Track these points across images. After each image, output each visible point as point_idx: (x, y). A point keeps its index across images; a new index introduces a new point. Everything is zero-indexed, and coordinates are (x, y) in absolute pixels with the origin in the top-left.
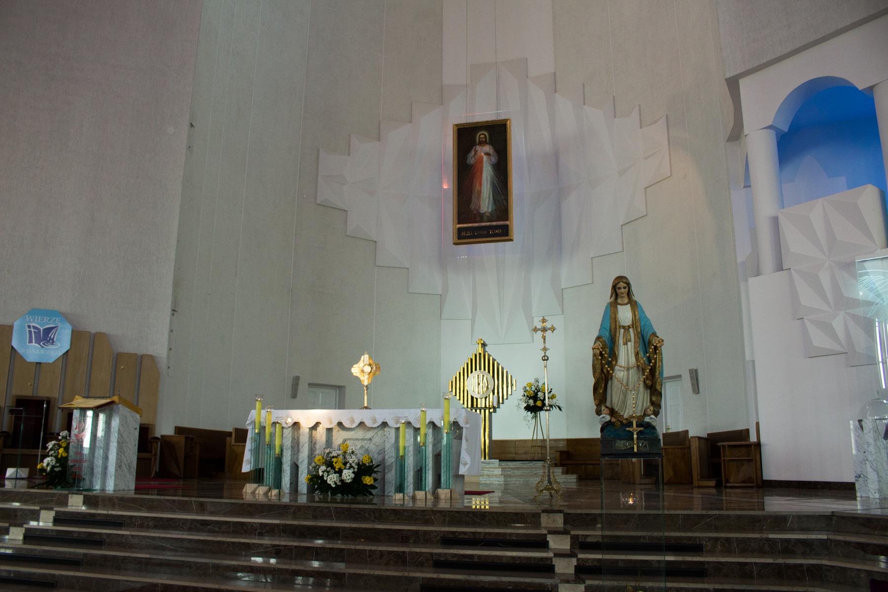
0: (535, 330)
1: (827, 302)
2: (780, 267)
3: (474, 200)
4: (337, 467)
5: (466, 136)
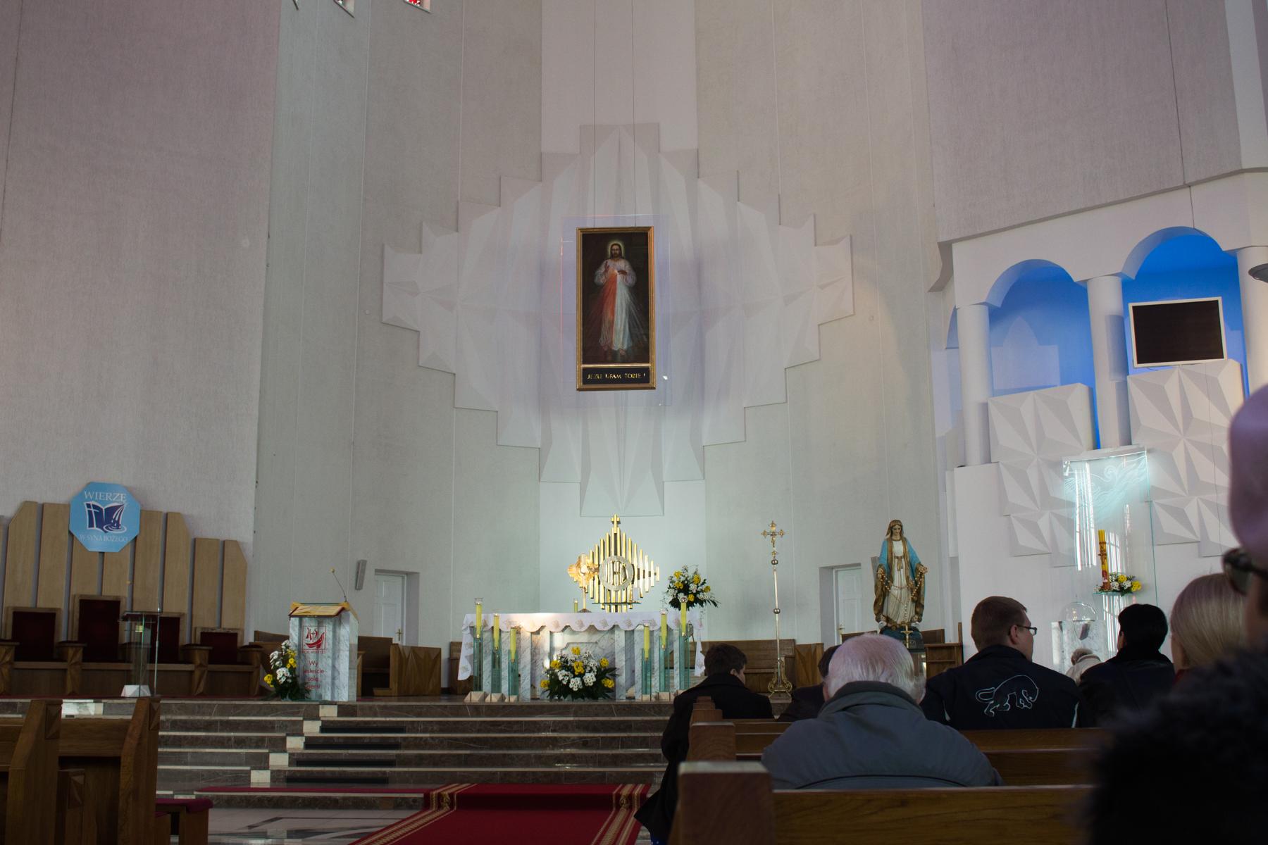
1: (1035, 501)
2: (988, 460)
3: (604, 332)
4: (577, 671)
5: (594, 245)
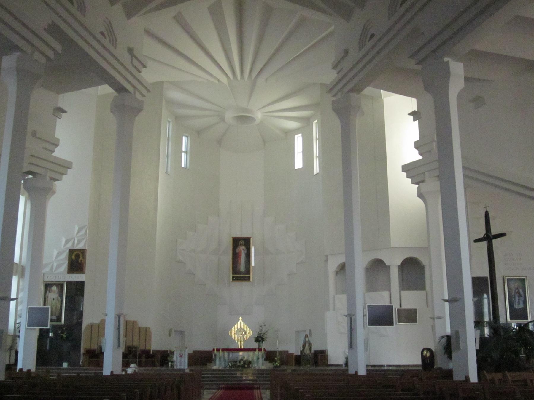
0: (439, 318)
5: (236, 241)
